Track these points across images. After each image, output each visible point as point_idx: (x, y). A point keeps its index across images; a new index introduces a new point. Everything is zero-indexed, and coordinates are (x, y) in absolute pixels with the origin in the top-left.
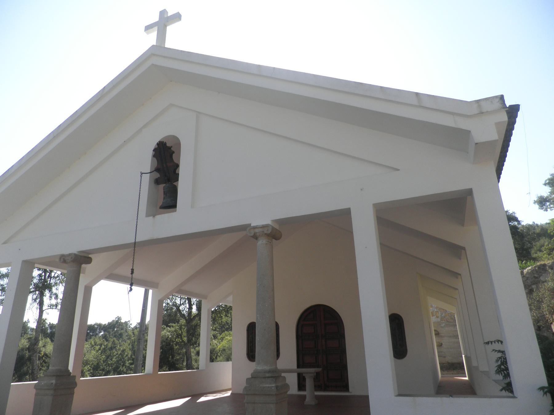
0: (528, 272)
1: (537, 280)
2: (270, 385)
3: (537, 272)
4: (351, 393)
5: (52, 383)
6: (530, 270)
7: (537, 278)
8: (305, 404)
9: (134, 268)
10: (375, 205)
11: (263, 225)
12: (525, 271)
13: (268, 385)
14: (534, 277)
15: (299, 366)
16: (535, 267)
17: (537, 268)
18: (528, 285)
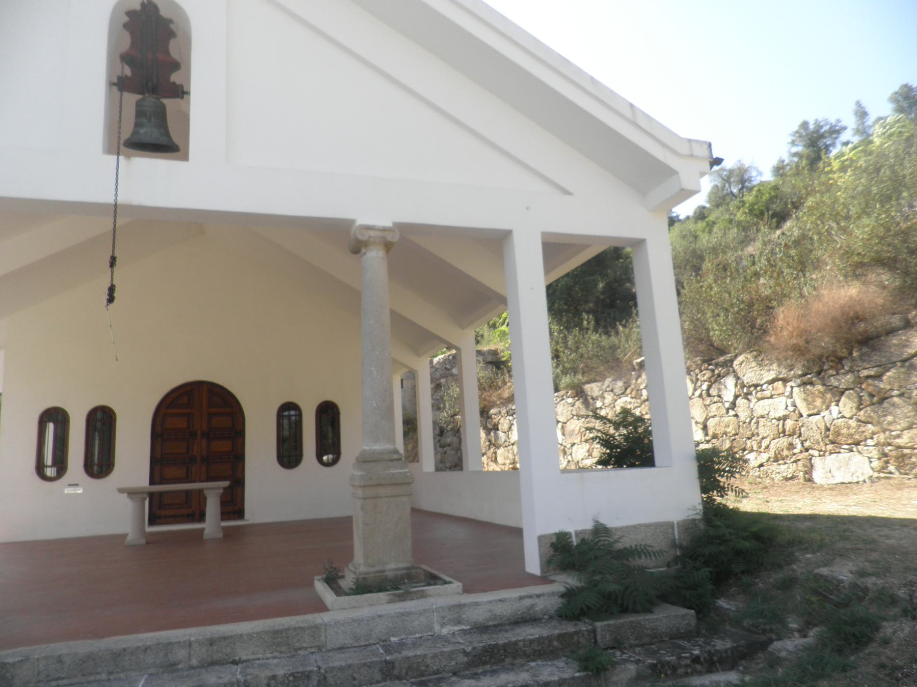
0: (438, 362)
1: (448, 372)
2: (401, 471)
3: (450, 362)
4: (248, 520)
5: (579, 408)
6: (442, 359)
7: (449, 370)
8: (205, 537)
9: (116, 255)
10: (545, 235)
11: (384, 227)
12: (436, 360)
13: (398, 471)
14: (446, 368)
15: (152, 482)
16: (449, 356)
17: (451, 358)
18: (436, 378)
